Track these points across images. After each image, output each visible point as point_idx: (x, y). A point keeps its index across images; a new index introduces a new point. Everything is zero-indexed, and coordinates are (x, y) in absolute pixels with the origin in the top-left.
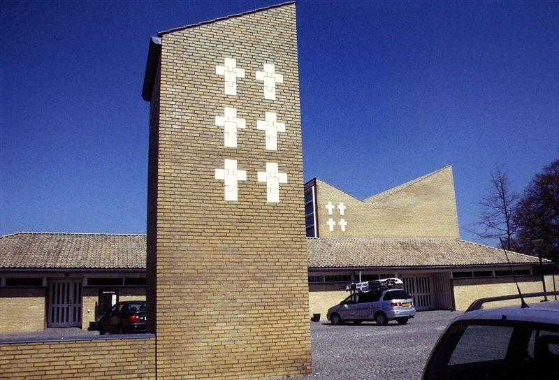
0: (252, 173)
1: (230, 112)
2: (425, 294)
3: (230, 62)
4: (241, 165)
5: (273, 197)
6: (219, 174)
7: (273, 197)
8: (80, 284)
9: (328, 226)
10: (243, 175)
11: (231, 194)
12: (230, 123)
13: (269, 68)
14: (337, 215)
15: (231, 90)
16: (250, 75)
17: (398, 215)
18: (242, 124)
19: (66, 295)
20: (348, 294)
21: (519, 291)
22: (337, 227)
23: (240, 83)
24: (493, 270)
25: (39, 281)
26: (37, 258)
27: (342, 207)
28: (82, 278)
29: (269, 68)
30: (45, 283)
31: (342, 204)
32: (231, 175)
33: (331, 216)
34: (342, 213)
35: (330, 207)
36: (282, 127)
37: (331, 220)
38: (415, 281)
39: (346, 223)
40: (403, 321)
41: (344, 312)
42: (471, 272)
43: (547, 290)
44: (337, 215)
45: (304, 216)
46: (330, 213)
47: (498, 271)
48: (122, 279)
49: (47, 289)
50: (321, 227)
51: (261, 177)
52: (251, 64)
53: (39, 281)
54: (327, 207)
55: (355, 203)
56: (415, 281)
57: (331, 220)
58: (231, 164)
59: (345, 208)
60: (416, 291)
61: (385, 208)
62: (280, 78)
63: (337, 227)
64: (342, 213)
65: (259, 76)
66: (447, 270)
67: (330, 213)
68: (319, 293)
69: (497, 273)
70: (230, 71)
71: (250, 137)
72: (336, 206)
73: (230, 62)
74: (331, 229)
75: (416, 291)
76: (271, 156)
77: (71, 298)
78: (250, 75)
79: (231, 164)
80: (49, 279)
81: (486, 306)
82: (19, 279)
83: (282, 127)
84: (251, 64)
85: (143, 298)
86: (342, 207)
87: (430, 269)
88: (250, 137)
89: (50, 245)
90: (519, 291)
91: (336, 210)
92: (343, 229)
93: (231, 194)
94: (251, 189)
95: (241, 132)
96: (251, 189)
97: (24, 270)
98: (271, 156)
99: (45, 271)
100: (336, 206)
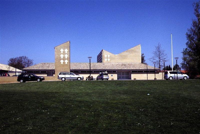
0: (64, 61)
1: (62, 55)
2: (127, 76)
3: (62, 49)
4: (63, 60)
5: (66, 63)
6: (61, 61)
7: (66, 63)
9: (105, 60)
10: (63, 61)
11: (62, 63)
12: (62, 56)
13: (66, 49)
14: (107, 58)
15: (62, 52)
16: (64, 51)
17: (125, 57)
20: (99, 75)
22: (107, 60)
23: (63, 52)
24: (112, 71)
25: (46, 72)
26: (45, 68)
27: (109, 56)
29: (66, 49)
30: (47, 72)
32: (62, 61)
35: (106, 56)
37: (106, 59)
38: (125, 73)
39: (110, 60)
43: (16, 71)
44: (107, 58)
46: (106, 57)
49: (47, 73)
50: (104, 60)
51: (65, 61)
52: (64, 49)
53: (46, 72)
55: (113, 55)
56: (125, 73)
57: (106, 59)
58: (62, 60)
62: (67, 50)
63: (107, 60)
64: (109, 57)
67: (106, 57)
69: (41, 72)
70: (62, 50)
71: (64, 57)
72: (107, 55)
73: (62, 49)
74: (106, 61)
76: (66, 59)
79: (62, 60)
80: (47, 71)
83: (67, 56)
84: (64, 49)
86: (109, 56)
88: (64, 57)
89: (47, 65)
92: (109, 61)
93: (62, 63)
94: (64, 63)
95: (63, 57)
96: (64, 63)
97: (43, 70)
98: (66, 59)
99: (47, 70)
100: (107, 55)
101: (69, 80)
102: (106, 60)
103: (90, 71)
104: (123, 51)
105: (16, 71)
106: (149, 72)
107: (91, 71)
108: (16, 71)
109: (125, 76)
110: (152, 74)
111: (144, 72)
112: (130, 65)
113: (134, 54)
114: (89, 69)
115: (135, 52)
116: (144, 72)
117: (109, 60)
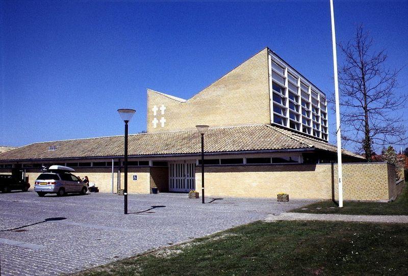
0: (159, 120)
8: (195, 164)
17: (211, 106)
19: (183, 170)
22: (159, 125)
25: (147, 163)
28: (196, 160)
30: (150, 164)
31: (163, 106)
33: (155, 117)
34: (163, 113)
35: (155, 109)
37: (155, 119)
39: (165, 121)
40: (88, 194)
42: (105, 163)
44: (159, 116)
47: (69, 163)
48: (270, 159)
54: (153, 110)
57: (155, 119)
60: (175, 175)
61: (195, 104)
64: (163, 113)
66: (193, 158)
68: (101, 173)
74: (155, 126)
75: (175, 175)
77: (186, 173)
82: (84, 163)
85: (11, 174)
86: (163, 108)
87: (234, 154)
91: (159, 111)
92: (163, 125)
101: (170, 184)
102: (155, 121)
103: (203, 157)
104: (206, 84)
105: (203, 150)
106: (135, 163)
107: (129, 160)
108: (203, 150)
109: (187, 178)
110: (279, 173)
111: (245, 162)
112: (52, 146)
113: (242, 91)
114: (122, 153)
115: (249, 80)
116: (245, 162)
117: (163, 120)
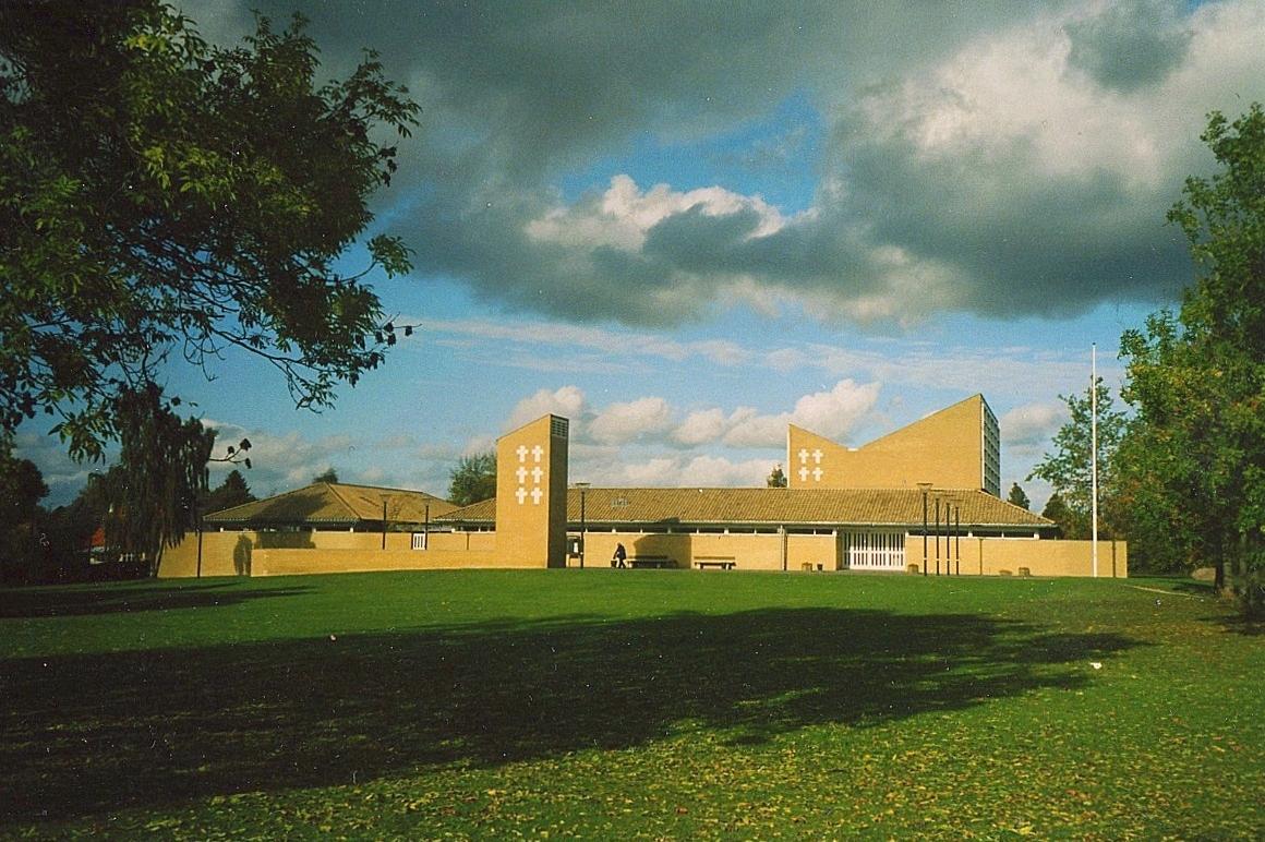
1: (522, 469)
5: (537, 501)
7: (537, 501)
16: (530, 452)
18: (526, 473)
21: (1114, 573)
36: (541, 473)
41: (189, 23)
45: (932, 570)
59: (822, 455)
65: (533, 473)
70: (522, 451)
71: (529, 478)
78: (530, 452)
81: (703, 547)
83: (541, 493)
84: (530, 447)
86: (818, 455)
88: (529, 478)
90: (1114, 573)
91: (811, 459)
94: (529, 498)
96: (529, 498)
